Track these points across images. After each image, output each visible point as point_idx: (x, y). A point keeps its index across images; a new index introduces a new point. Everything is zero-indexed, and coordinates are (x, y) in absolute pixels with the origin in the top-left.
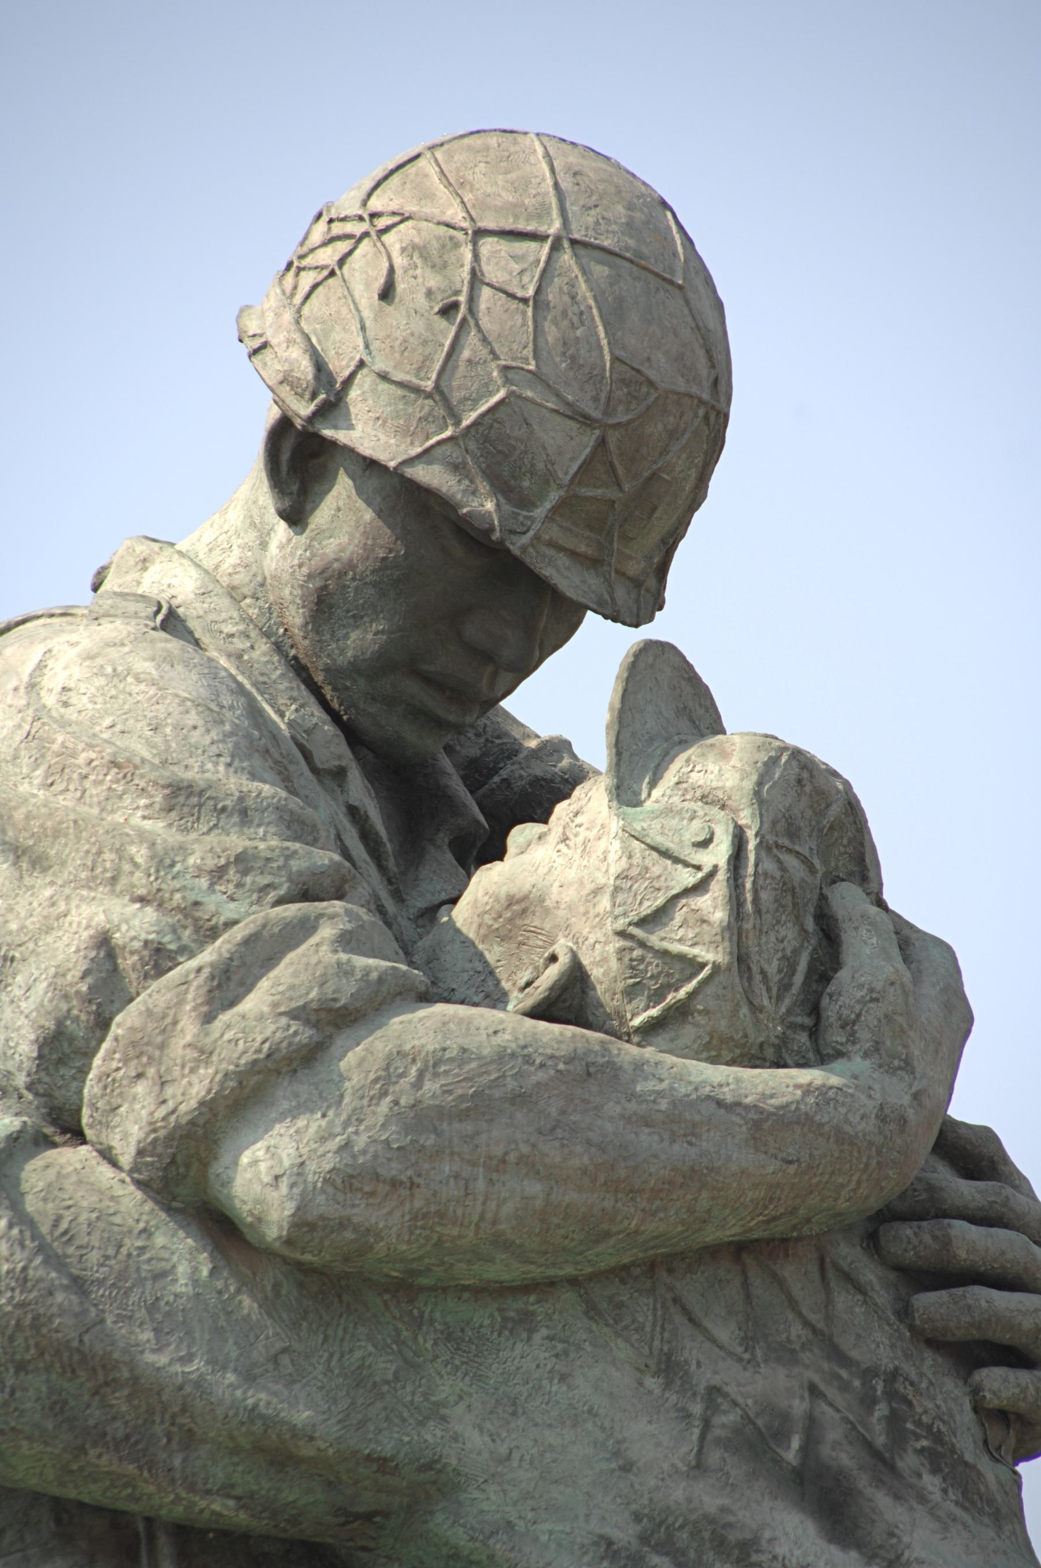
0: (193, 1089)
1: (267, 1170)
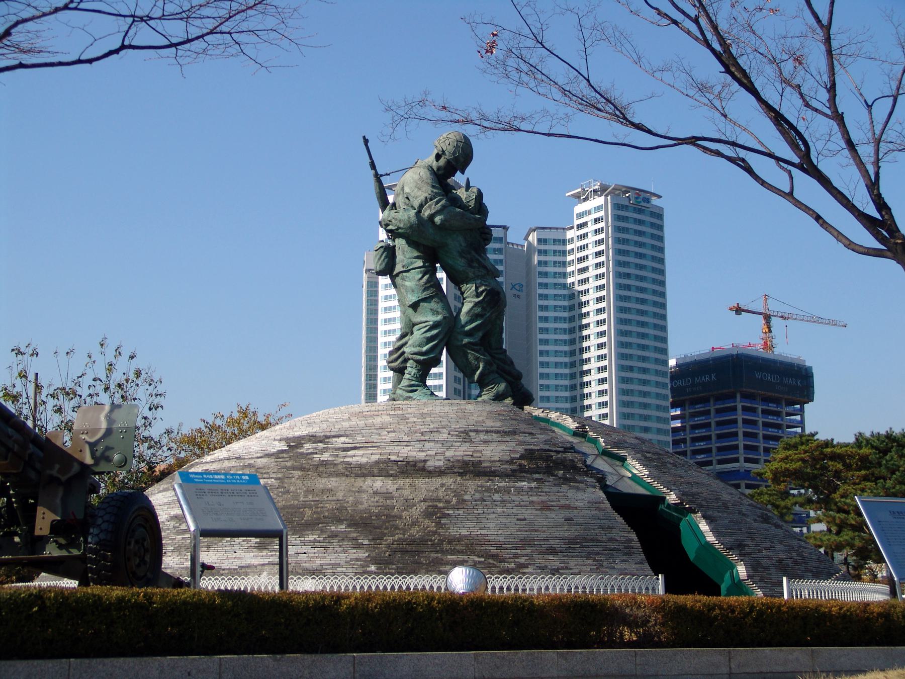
0: (433, 211)
1: (438, 219)
